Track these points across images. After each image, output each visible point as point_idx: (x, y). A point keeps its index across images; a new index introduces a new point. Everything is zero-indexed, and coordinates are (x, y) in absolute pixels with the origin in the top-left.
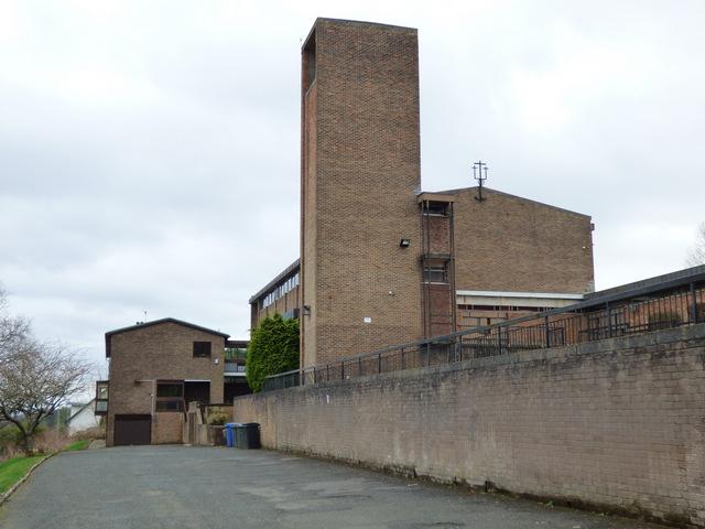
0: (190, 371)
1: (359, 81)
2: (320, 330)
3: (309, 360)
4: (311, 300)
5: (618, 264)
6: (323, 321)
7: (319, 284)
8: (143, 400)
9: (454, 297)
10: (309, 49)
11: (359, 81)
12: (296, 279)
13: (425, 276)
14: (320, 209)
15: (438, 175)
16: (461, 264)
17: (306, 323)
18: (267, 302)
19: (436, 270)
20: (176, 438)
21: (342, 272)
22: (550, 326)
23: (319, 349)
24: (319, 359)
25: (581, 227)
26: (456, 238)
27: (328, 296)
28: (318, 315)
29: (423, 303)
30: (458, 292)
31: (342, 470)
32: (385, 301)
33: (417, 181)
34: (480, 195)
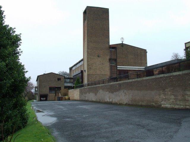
0: (54, 85)
1: (96, 20)
2: (88, 75)
3: (86, 81)
4: (86, 69)
5: (152, 60)
6: (89, 73)
7: (88, 65)
8: (46, 91)
9: (117, 68)
10: (85, 13)
11: (96, 20)
12: (82, 63)
13: (110, 63)
14: (88, 48)
15: (114, 40)
16: (118, 60)
17: (85, 74)
18: (73, 69)
19: (113, 61)
20: (54, 99)
21: (93, 63)
22: (139, 74)
23: (88, 79)
24: (88, 81)
25: (144, 52)
26: (117, 55)
27: (89, 68)
28: (88, 72)
29: (110, 69)
30: (118, 67)
31: (87, 103)
32: (104, 69)
33: (108, 42)
34: (122, 45)
